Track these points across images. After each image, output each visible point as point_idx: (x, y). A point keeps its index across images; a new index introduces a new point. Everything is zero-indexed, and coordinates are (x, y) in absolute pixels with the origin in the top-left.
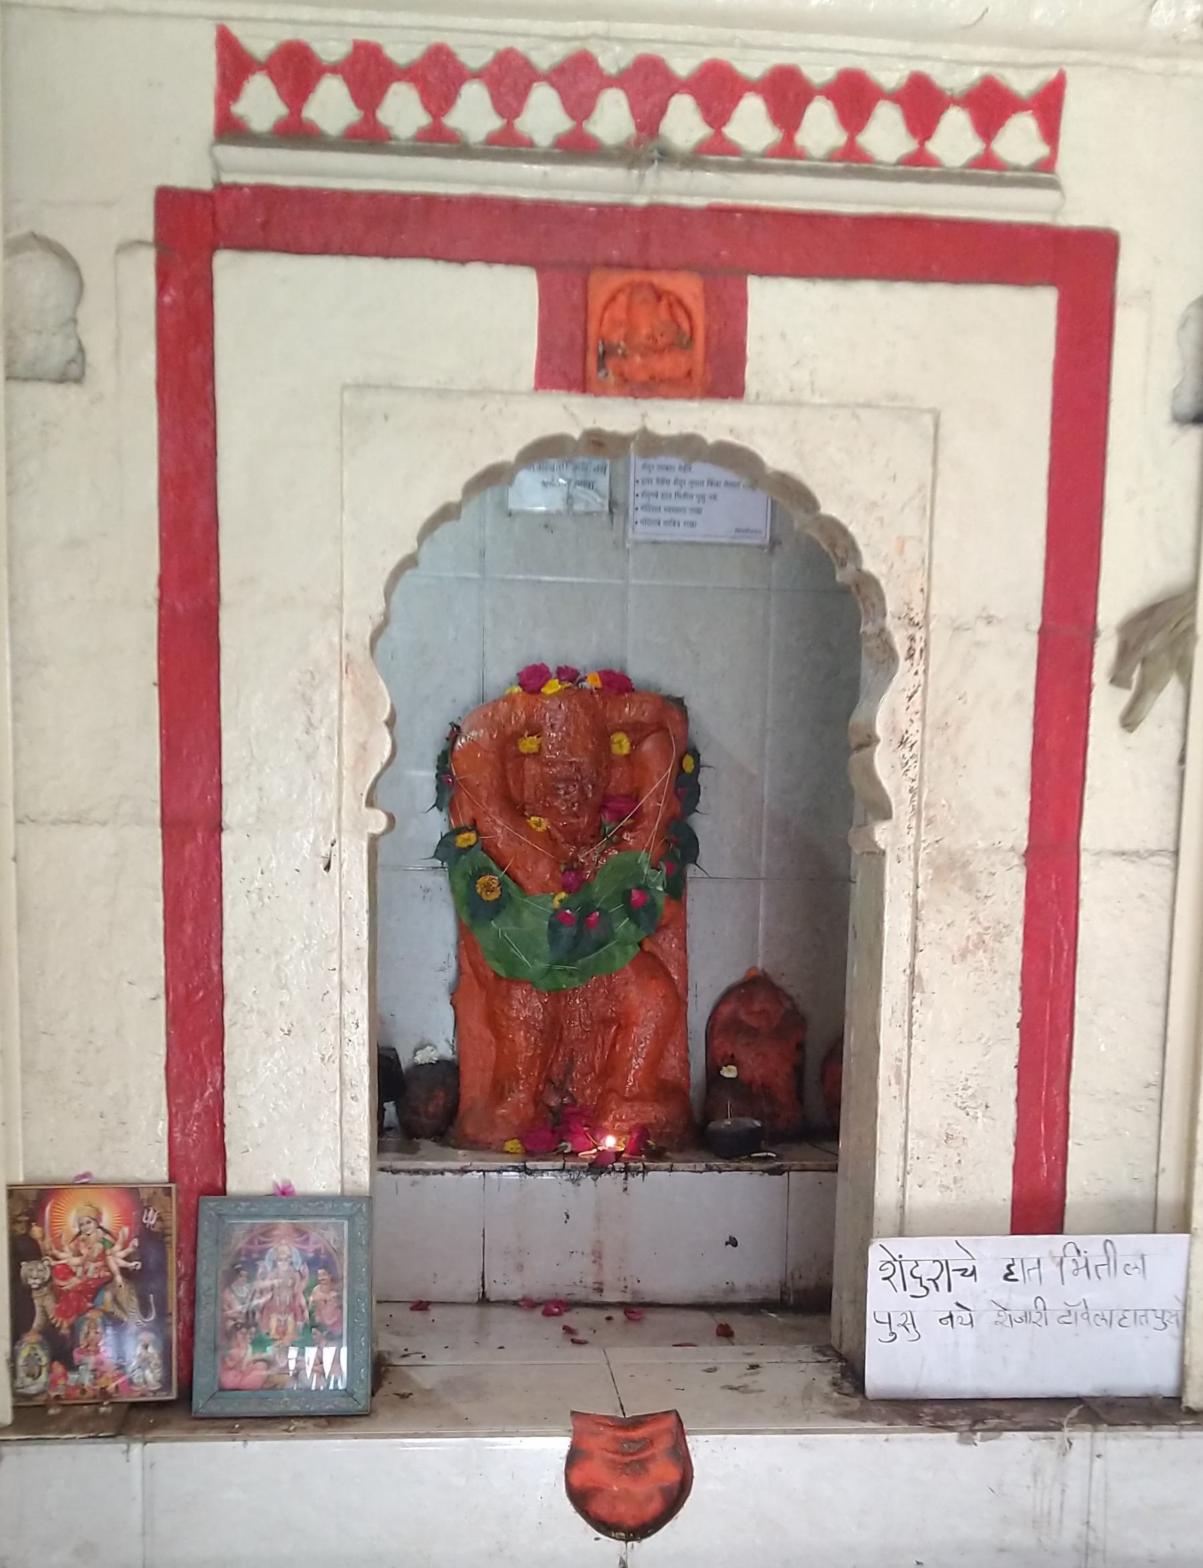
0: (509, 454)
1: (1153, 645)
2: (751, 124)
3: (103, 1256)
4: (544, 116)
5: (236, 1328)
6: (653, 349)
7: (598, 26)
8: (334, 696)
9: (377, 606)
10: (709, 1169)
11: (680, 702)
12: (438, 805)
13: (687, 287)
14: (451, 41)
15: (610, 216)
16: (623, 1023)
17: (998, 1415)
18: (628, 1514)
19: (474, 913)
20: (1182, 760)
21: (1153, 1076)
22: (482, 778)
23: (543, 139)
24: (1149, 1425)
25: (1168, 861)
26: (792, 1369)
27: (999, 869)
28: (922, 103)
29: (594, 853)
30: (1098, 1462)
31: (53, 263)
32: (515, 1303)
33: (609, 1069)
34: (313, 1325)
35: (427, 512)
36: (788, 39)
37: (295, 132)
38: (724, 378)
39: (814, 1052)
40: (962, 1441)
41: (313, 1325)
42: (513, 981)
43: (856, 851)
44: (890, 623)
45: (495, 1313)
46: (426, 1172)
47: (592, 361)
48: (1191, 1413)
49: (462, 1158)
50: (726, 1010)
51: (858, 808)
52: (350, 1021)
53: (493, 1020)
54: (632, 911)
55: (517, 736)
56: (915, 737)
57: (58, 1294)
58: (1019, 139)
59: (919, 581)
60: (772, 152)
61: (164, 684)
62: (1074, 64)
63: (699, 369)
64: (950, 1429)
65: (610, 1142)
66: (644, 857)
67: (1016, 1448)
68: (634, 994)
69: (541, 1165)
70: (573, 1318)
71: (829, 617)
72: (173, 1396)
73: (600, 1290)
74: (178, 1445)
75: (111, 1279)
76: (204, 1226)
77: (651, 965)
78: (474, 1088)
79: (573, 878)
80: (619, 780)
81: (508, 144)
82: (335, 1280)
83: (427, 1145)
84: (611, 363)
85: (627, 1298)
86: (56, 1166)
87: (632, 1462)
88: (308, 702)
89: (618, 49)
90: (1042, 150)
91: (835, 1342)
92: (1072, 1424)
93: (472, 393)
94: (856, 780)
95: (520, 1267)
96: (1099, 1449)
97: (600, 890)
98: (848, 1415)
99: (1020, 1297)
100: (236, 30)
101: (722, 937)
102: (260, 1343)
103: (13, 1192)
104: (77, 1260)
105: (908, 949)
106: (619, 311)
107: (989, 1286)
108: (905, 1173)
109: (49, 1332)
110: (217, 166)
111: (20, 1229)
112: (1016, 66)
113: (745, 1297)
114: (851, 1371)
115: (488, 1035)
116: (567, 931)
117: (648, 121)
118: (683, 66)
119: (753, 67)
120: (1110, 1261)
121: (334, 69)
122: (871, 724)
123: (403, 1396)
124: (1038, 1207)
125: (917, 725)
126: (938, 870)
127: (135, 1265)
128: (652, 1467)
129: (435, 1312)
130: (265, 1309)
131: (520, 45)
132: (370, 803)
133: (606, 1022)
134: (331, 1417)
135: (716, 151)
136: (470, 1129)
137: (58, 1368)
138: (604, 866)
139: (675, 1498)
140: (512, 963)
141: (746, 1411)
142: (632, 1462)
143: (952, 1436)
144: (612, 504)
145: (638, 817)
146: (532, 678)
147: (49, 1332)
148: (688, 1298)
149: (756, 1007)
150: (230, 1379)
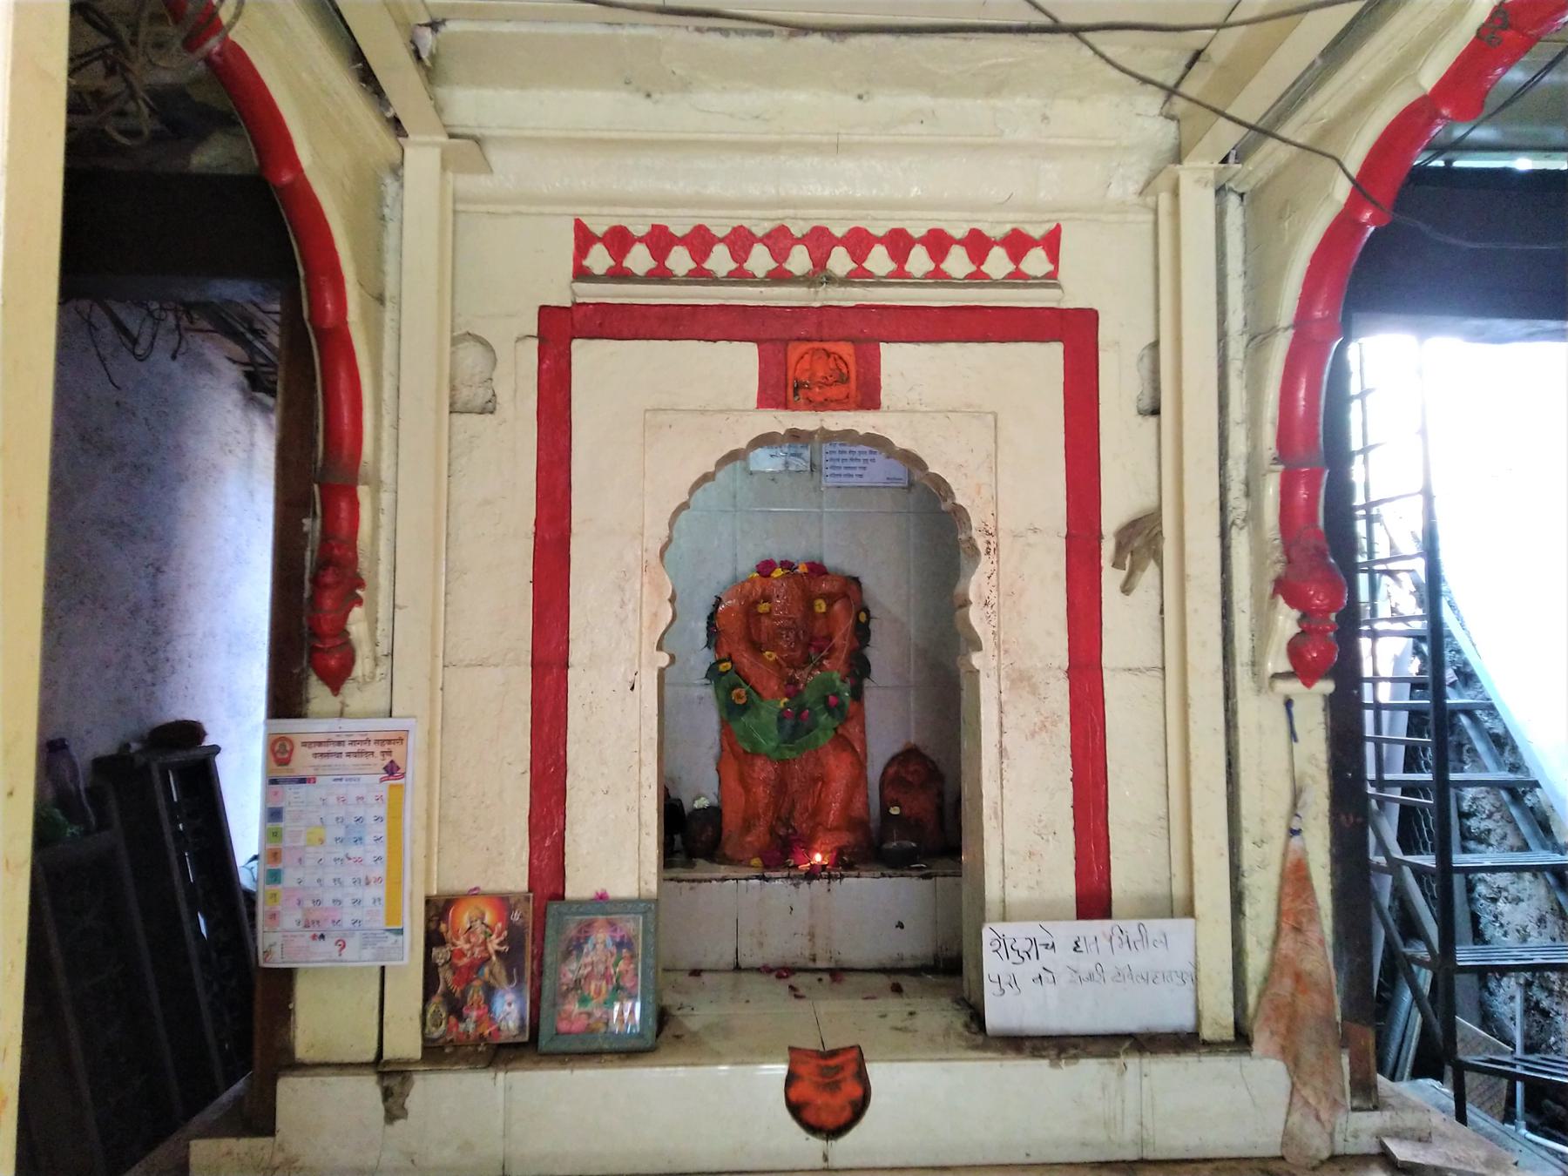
0: (743, 444)
1: (1137, 543)
2: (879, 261)
3: (484, 943)
4: (760, 260)
5: (569, 990)
6: (826, 384)
7: (790, 212)
8: (638, 586)
9: (664, 532)
10: (883, 875)
11: (856, 580)
12: (708, 645)
13: (845, 350)
14: (707, 223)
15: (799, 313)
16: (823, 780)
17: (1075, 1047)
18: (829, 1121)
19: (731, 711)
20: (1162, 612)
21: (1162, 812)
22: (732, 626)
23: (760, 274)
24: (1177, 1053)
25: (1159, 674)
26: (936, 1015)
27: (1052, 681)
28: (978, 245)
29: (804, 673)
30: (1145, 1080)
31: (479, 348)
32: (758, 970)
33: (817, 811)
34: (618, 988)
35: (694, 478)
36: (898, 214)
37: (618, 274)
38: (869, 398)
39: (949, 799)
40: (1054, 1065)
41: (618, 988)
42: (756, 754)
43: (963, 671)
44: (975, 534)
45: (743, 975)
46: (700, 881)
47: (790, 391)
48: (1206, 1043)
49: (723, 871)
50: (892, 771)
51: (963, 645)
52: (645, 784)
53: (743, 780)
54: (829, 709)
55: (756, 603)
56: (993, 601)
57: (455, 970)
58: (1036, 262)
59: (991, 508)
60: (891, 275)
61: (536, 581)
62: (1069, 219)
63: (853, 393)
64: (1043, 1057)
65: (818, 858)
66: (836, 675)
67: (1089, 1070)
68: (832, 761)
69: (773, 874)
70: (796, 980)
71: (938, 529)
72: (526, 1038)
73: (814, 960)
74: (528, 1073)
75: (490, 958)
76: (550, 921)
77: (842, 742)
78: (731, 820)
79: (792, 688)
80: (819, 627)
81: (740, 276)
82: (633, 956)
83: (701, 862)
84: (801, 392)
85: (832, 965)
86: (457, 882)
87: (831, 1084)
88: (622, 590)
89: (801, 223)
90: (1051, 267)
91: (966, 994)
92: (1126, 1052)
93: (721, 411)
94: (959, 627)
95: (761, 944)
96: (1145, 1070)
97: (809, 696)
98: (976, 1048)
99: (1085, 963)
100: (585, 221)
101: (887, 726)
102: (584, 1001)
103: (429, 901)
104: (467, 946)
105: (997, 732)
106: (805, 364)
107: (1064, 952)
108: (1004, 878)
109: (448, 994)
110: (574, 293)
111: (433, 926)
112: (1030, 222)
113: (909, 963)
114: (976, 1016)
115: (740, 789)
116: (789, 723)
117: (820, 262)
118: (839, 231)
119: (879, 230)
120: (1144, 937)
121: (641, 240)
122: (966, 594)
123: (678, 1037)
124: (1094, 901)
125: (995, 593)
126: (1013, 681)
127: (505, 948)
128: (843, 1086)
129: (705, 977)
130: (588, 977)
131: (746, 224)
132: (660, 648)
133: (815, 780)
134: (629, 1052)
135: (860, 276)
136: (729, 853)
137: (453, 1019)
138: (810, 678)
139: (860, 1107)
140: (754, 743)
141: (907, 1045)
142: (831, 1084)
143: (1045, 1062)
144: (812, 465)
145: (832, 650)
146: (765, 568)
147: (448, 994)
148: (873, 964)
149: (911, 769)
150: (563, 1026)
